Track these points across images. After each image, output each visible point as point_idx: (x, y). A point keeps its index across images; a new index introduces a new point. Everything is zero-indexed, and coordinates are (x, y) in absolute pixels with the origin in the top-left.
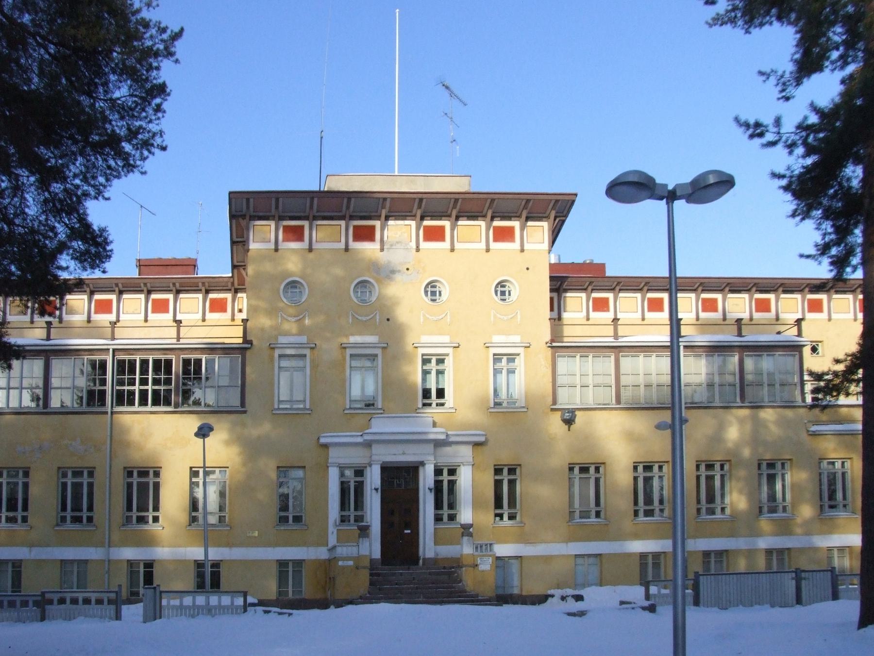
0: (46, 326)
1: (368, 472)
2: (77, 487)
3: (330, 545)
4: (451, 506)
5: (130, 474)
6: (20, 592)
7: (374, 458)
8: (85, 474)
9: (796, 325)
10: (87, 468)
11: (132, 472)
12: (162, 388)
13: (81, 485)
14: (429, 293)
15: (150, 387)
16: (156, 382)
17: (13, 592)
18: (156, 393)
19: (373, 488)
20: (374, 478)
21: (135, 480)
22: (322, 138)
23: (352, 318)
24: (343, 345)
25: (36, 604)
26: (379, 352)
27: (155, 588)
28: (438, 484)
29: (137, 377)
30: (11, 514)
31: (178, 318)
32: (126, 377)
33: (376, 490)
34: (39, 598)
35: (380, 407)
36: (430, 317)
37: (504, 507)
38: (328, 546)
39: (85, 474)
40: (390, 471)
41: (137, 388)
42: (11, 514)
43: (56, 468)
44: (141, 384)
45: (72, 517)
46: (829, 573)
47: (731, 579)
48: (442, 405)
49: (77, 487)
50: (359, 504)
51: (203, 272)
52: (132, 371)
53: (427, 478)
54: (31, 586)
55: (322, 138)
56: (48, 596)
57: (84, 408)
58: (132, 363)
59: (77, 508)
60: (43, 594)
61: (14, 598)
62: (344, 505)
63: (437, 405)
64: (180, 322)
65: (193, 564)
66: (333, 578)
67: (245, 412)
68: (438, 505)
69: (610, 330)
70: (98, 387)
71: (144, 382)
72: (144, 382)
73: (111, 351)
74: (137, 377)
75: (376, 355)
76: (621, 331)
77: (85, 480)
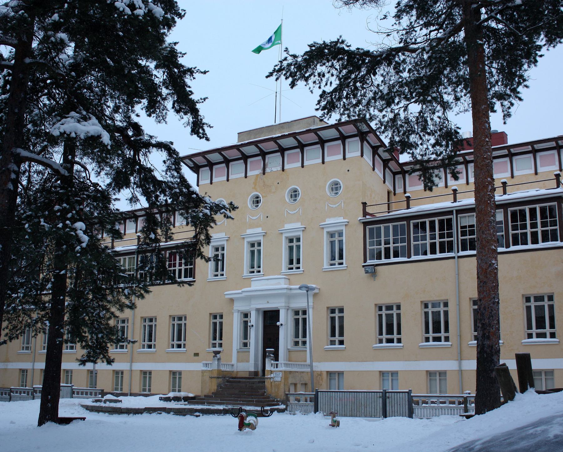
2: (390, 317)
5: (426, 306)
8: (395, 308)
10: (395, 303)
15: (437, 240)
16: (442, 236)
21: (430, 310)
23: (287, 214)
26: (343, 228)
30: (389, 337)
36: (334, 206)
37: (554, 331)
39: (395, 308)
42: (389, 337)
44: (431, 239)
46: (407, 394)
47: (351, 396)
48: (342, 264)
49: (390, 317)
52: (523, 218)
58: (523, 213)
71: (534, 226)
72: (534, 226)
73: (454, 212)
77: (394, 312)
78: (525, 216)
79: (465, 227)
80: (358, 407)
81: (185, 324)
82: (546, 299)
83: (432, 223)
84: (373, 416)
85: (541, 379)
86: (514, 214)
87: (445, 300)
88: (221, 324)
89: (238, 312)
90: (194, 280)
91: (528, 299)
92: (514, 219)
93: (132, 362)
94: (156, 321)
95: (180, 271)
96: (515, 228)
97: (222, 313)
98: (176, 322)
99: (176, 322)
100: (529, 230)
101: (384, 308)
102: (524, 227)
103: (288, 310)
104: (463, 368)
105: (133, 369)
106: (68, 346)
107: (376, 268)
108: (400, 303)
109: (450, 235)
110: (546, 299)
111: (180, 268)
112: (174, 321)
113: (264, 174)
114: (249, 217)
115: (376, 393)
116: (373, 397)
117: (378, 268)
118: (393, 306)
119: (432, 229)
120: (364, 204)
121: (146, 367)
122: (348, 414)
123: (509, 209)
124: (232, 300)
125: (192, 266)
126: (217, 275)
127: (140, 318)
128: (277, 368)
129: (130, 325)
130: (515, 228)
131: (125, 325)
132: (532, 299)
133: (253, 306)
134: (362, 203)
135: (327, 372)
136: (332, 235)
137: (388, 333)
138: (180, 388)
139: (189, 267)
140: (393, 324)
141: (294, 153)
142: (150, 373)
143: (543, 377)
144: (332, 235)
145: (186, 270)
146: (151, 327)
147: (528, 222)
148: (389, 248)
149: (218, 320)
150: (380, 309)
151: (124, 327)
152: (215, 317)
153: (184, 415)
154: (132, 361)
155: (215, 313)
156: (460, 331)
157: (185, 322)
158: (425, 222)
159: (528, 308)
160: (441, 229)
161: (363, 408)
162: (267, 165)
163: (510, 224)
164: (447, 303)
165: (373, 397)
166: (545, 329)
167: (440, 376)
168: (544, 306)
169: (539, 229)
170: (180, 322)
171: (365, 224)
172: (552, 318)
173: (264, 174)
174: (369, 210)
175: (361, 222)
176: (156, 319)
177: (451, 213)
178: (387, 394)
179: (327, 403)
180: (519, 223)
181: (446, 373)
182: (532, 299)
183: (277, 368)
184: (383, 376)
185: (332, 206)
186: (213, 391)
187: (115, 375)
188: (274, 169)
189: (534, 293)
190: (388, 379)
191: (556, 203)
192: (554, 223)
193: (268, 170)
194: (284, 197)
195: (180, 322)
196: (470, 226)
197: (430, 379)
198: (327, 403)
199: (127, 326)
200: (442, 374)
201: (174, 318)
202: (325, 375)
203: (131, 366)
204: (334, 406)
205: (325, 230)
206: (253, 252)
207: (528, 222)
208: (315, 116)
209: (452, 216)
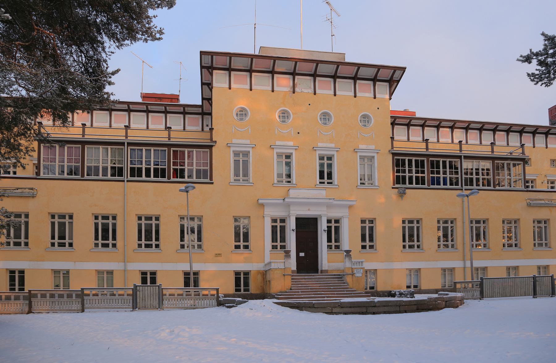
0: (82, 126)
1: (287, 221)
2: (411, 229)
3: (266, 262)
4: (337, 240)
6: (69, 289)
7: (291, 212)
9: (521, 147)
11: (55, 215)
12: (179, 167)
13: (64, 224)
14: (322, 119)
15: (448, 176)
16: (417, 172)
17: (63, 289)
18: (417, 178)
19: (291, 229)
20: (292, 224)
21: (57, 220)
22: (255, 28)
24: (314, 148)
25: (77, 296)
27: (159, 286)
28: (329, 228)
29: (66, 157)
30: (411, 243)
31: (168, 126)
32: (420, 169)
33: (293, 230)
34: (80, 293)
35: (377, 185)
38: (264, 263)
40: (300, 221)
41: (144, 166)
43: (28, 211)
45: (59, 243)
46: (550, 277)
50: (283, 239)
51: (182, 101)
52: (438, 167)
53: (323, 226)
54: (75, 285)
55: (255, 28)
56: (86, 292)
57: (66, 176)
58: (404, 161)
59: (62, 237)
60: (82, 289)
61: (19, 294)
62: (274, 239)
63: (328, 183)
64: (427, 140)
65: (50, 271)
66: (269, 281)
67: (212, 183)
68: (329, 240)
69: (489, 148)
70: (469, 176)
74: (66, 157)
75: (373, 157)
76: (173, 134)
78: (405, 164)
80: (515, 289)
82: (154, 219)
83: (410, 162)
84: (519, 295)
85: (60, 276)
87: (26, 212)
90: (212, 182)
91: (96, 218)
92: (175, 157)
96: (432, 172)
102: (438, 173)
104: (123, 264)
109: (423, 172)
110: (111, 218)
113: (294, 92)
114: (373, 133)
115: (494, 279)
116: (527, 281)
117: (407, 190)
119: (444, 167)
122: (508, 295)
123: (171, 149)
130: (175, 164)
132: (143, 219)
136: (236, 154)
140: (152, 230)
141: (364, 84)
144: (236, 154)
147: (407, 169)
148: (412, 176)
150: (53, 217)
153: (302, 310)
159: (53, 224)
161: (519, 289)
162: (296, 85)
163: (172, 161)
165: (527, 281)
166: (65, 240)
168: (108, 224)
172: (114, 231)
173: (294, 92)
178: (138, 288)
179: (490, 288)
180: (435, 170)
181: (69, 271)
186: (287, 288)
189: (52, 212)
192: (423, 172)
193: (297, 89)
198: (490, 288)
204: (496, 289)
207: (441, 170)
209: (124, 147)
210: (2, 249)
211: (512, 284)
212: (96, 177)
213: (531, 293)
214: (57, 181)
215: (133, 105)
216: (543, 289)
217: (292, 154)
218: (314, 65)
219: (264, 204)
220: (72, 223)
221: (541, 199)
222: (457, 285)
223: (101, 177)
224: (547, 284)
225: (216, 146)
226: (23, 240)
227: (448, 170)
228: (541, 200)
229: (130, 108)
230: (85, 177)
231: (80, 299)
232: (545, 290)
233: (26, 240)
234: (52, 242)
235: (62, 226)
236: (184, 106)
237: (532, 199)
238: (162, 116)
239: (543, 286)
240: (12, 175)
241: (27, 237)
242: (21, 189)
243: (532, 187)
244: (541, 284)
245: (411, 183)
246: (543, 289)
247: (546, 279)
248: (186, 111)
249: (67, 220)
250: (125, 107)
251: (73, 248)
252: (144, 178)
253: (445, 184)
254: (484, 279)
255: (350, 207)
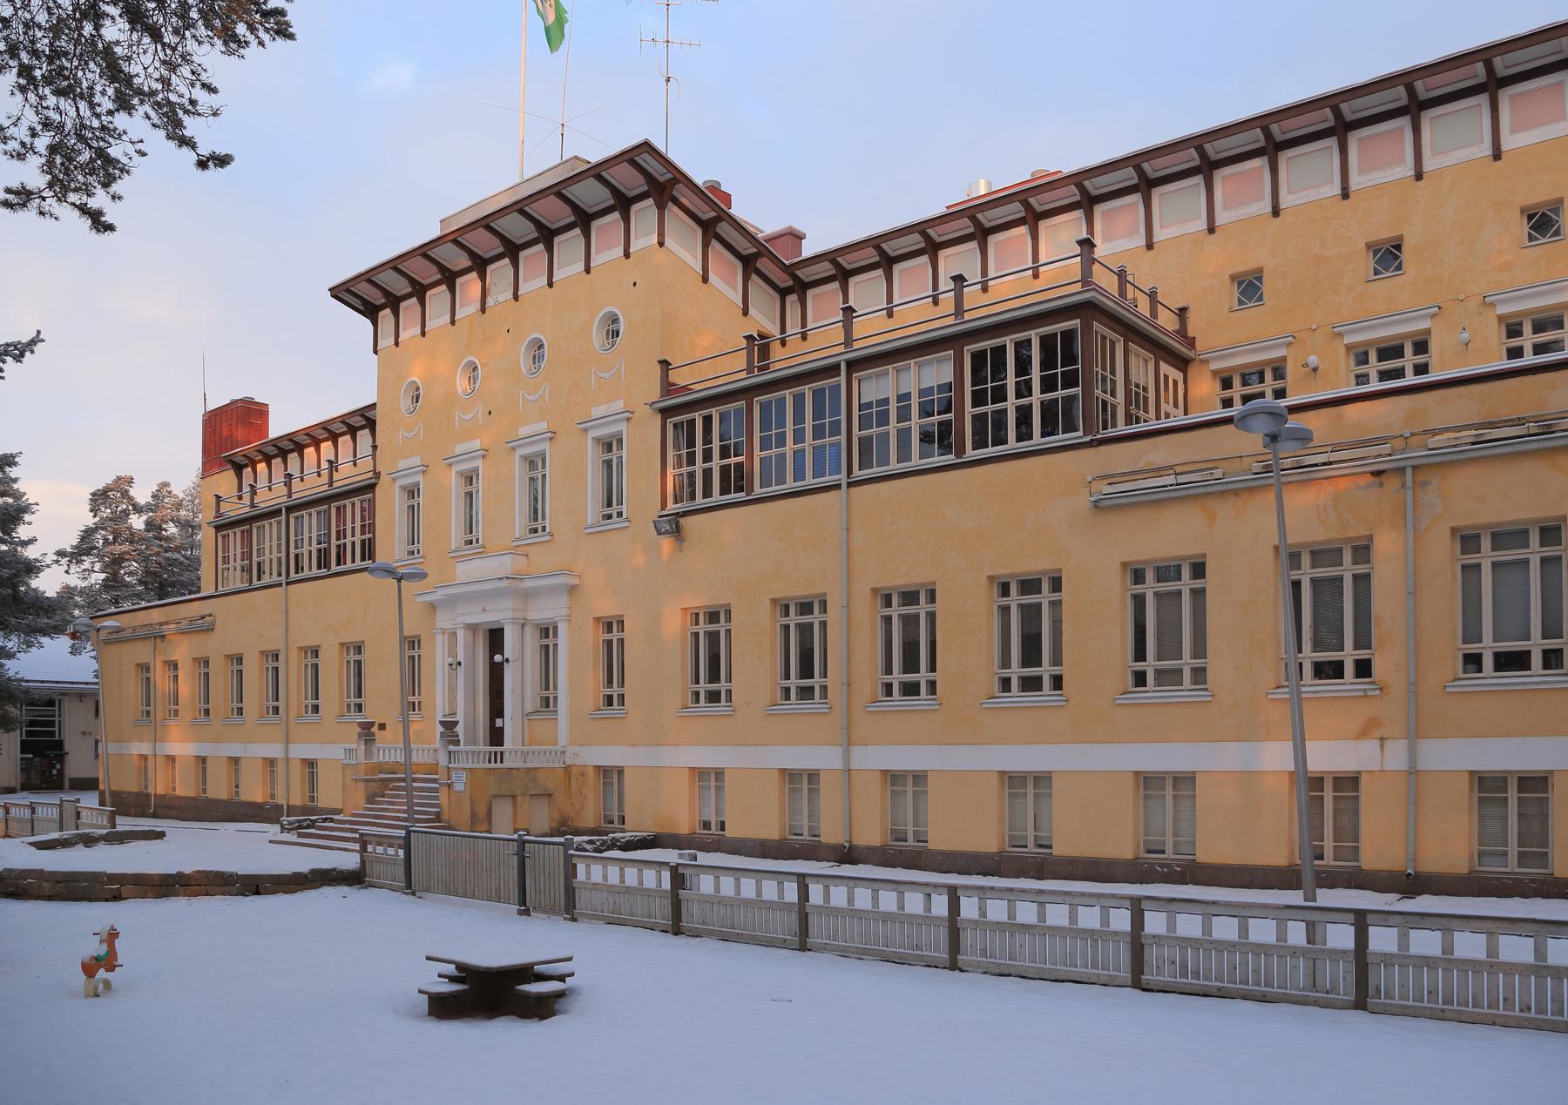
2: (910, 622)
8: (1045, 587)
12: (913, 423)
21: (1150, 588)
39: (1045, 587)
44: (1019, 395)
71: (1024, 390)
72: (1024, 390)
79: (869, 405)
81: (728, 632)
86: (978, 358)
88: (621, 641)
89: (444, 633)
93: (849, 744)
94: (728, 619)
95: (707, 474)
97: (1060, 570)
98: (794, 619)
99: (794, 619)
100: (1011, 403)
101: (1013, 589)
103: (523, 626)
104: (1423, 765)
105: (853, 767)
106: (697, 694)
107: (682, 521)
108: (1204, 555)
111: (707, 465)
112: (787, 614)
113: (483, 310)
118: (1040, 580)
119: (1023, 366)
120: (665, 363)
121: (234, 749)
124: (433, 607)
125: (741, 459)
126: (609, 517)
127: (296, 649)
128: (502, 762)
129: (834, 615)
131: (721, 627)
133: (461, 620)
134: (660, 362)
135: (598, 768)
137: (1318, 645)
138: (623, 811)
139: (733, 460)
141: (534, 254)
142: (620, 771)
143: (1030, 790)
145: (725, 470)
146: (805, 630)
147: (1011, 380)
149: (615, 636)
151: (718, 633)
152: (609, 627)
154: (848, 743)
155: (888, 588)
156: (849, 673)
157: (823, 617)
158: (1004, 347)
160: (1047, 363)
164: (1060, 579)
167: (1175, 788)
169: (893, 425)
170: (806, 619)
171: (666, 412)
174: (674, 377)
175: (655, 410)
176: (728, 613)
177: (833, 370)
180: (1059, 370)
182: (1150, 576)
183: (502, 762)
184: (893, 784)
185: (602, 375)
187: (1007, 791)
188: (501, 298)
190: (801, 790)
191: (1078, 321)
193: (490, 301)
194: (519, 361)
195: (806, 619)
196: (941, 388)
197: (1146, 797)
199: (824, 624)
200: (813, 776)
201: (787, 607)
202: (591, 773)
203: (287, 750)
205: (592, 434)
206: (608, 463)
207: (1011, 380)
208: (576, 158)
210: (1120, 702)
211: (468, 858)
212: (741, 496)
213: (493, 895)
214: (769, 503)
215: (1151, 162)
216: (542, 886)
217: (520, 456)
218: (533, 232)
219: (435, 604)
220: (1367, 577)
221: (1159, 469)
222: (1149, 917)
223: (1012, 444)
224: (552, 871)
225: (380, 484)
226: (1187, 662)
227: (1036, 374)
228: (1158, 471)
229: (1417, 97)
230: (668, 508)
231: (358, 845)
232: (547, 891)
233: (1198, 662)
234: (1136, 669)
235: (1031, 614)
236: (831, 256)
237: (1113, 476)
238: (1401, 129)
239: (542, 875)
240: (1410, 379)
241: (1200, 650)
242: (1447, 430)
243: (1421, 369)
244: (537, 869)
245: (1024, 434)
246: (542, 886)
247: (551, 851)
248: (1279, 136)
249: (1186, 583)
250: (1128, 176)
251: (1206, 690)
252: (1012, 444)
253: (1024, 434)
254: (414, 831)
255: (572, 589)
